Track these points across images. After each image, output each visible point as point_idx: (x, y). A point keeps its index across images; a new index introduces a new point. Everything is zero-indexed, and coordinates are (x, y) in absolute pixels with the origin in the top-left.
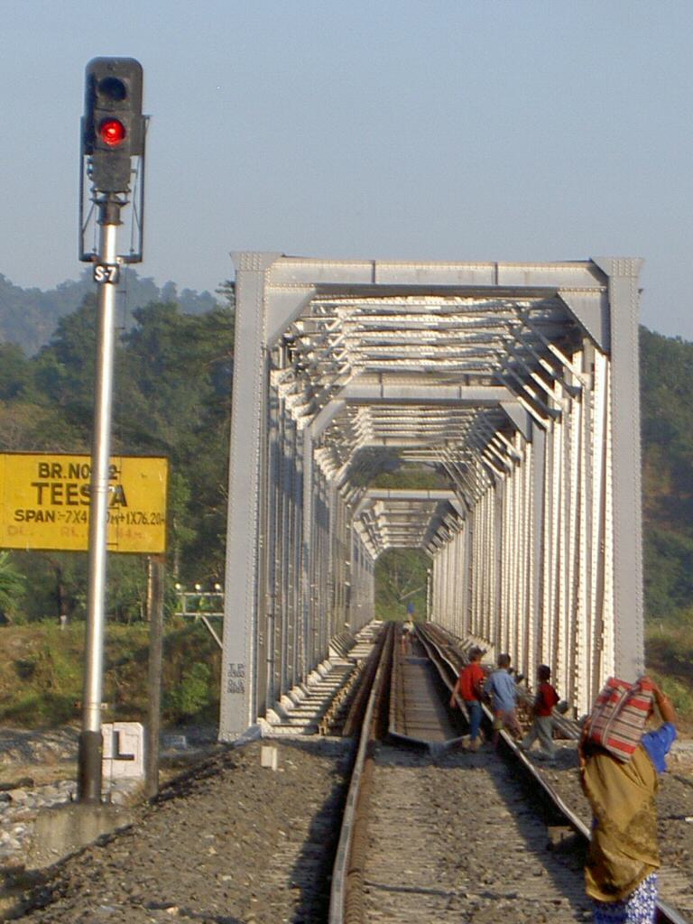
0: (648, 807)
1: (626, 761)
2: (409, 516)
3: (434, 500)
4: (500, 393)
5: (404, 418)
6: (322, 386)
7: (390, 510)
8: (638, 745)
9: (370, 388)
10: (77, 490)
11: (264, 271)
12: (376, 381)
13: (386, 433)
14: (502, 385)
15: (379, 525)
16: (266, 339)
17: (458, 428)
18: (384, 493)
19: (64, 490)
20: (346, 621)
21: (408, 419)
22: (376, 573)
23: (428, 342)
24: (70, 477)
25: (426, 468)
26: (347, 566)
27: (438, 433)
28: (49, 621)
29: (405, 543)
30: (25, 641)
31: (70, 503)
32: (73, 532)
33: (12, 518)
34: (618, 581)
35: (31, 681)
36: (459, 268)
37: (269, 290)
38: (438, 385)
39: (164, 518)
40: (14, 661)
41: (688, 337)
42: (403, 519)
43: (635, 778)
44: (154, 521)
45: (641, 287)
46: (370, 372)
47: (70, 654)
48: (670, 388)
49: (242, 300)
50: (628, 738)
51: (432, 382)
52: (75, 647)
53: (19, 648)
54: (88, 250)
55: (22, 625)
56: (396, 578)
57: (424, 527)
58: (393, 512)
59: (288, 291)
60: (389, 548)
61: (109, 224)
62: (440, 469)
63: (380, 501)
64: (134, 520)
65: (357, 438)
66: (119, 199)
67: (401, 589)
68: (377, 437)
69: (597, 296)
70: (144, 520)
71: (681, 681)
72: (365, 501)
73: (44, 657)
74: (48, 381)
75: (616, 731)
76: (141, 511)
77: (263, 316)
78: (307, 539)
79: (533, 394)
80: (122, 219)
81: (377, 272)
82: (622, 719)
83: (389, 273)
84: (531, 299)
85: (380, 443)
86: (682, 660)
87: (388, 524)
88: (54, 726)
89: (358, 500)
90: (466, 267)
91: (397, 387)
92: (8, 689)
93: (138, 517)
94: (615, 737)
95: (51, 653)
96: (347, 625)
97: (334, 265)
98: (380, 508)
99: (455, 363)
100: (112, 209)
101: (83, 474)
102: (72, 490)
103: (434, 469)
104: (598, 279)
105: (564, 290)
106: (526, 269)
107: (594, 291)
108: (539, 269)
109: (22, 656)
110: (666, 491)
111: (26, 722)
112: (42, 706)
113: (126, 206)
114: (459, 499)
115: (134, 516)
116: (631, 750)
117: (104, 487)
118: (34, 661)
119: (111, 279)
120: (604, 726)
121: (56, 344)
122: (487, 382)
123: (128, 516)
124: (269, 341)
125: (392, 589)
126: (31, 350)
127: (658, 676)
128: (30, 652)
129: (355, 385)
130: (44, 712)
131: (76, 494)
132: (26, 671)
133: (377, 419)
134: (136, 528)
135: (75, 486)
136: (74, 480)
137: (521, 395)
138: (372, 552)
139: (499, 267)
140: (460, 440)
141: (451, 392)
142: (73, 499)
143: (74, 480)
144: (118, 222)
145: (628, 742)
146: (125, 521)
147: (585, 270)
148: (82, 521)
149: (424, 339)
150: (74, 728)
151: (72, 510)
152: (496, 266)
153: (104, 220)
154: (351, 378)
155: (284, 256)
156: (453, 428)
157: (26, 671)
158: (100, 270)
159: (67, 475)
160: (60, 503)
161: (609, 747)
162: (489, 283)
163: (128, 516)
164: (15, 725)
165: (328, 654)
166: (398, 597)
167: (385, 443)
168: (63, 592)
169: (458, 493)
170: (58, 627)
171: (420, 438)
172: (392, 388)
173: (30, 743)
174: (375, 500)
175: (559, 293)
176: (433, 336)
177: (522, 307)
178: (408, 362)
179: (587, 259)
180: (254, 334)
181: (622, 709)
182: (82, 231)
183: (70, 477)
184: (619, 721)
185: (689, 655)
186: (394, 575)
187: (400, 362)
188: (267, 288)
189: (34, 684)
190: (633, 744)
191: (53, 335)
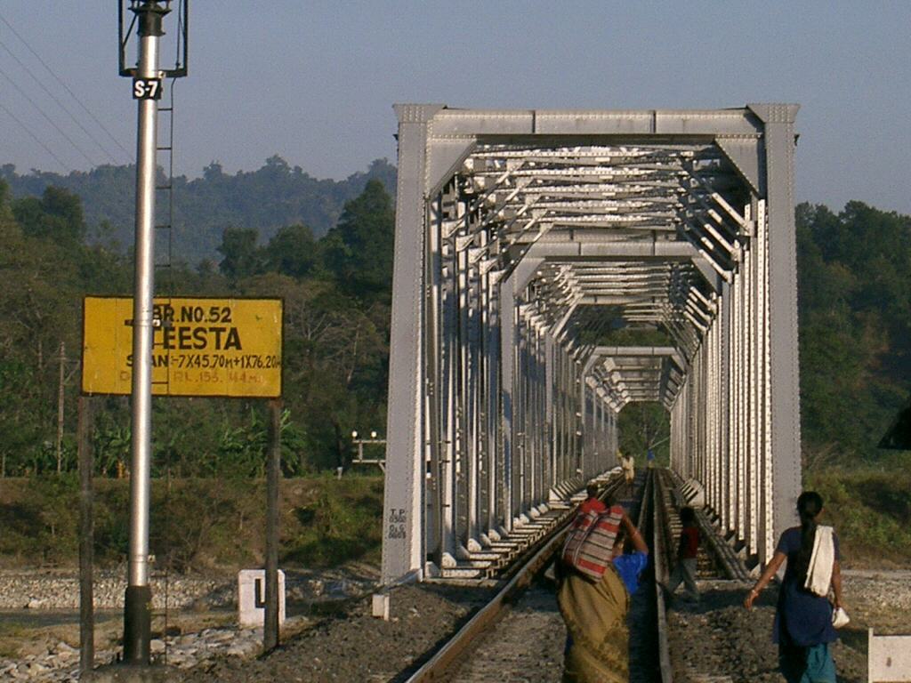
0: (620, 625)
1: (596, 580)
2: (641, 371)
3: (658, 356)
4: (685, 247)
5: (608, 276)
6: (509, 243)
7: (621, 366)
8: (609, 565)
9: (563, 245)
10: (191, 333)
11: (425, 123)
12: (568, 237)
13: (595, 291)
14: (686, 240)
15: (613, 381)
16: (428, 189)
17: (660, 285)
18: (612, 350)
19: (176, 333)
20: (578, 467)
21: (612, 276)
22: (620, 425)
23: (608, 197)
24: (183, 320)
25: (648, 327)
26: (578, 417)
27: (643, 290)
28: (327, 472)
29: (644, 397)
30: (306, 490)
31: (182, 347)
32: (187, 376)
33: (125, 365)
34: (775, 422)
35: (311, 526)
36: (618, 116)
37: (431, 141)
38: (626, 241)
39: (280, 360)
40: (295, 507)
41: (904, 211)
42: (636, 374)
43: (607, 597)
44: (269, 364)
45: (797, 133)
46: (558, 229)
47: (346, 501)
48: (887, 256)
49: (403, 151)
50: (599, 559)
51: (621, 239)
52: (350, 495)
53: (301, 496)
54: (130, 64)
55: (303, 476)
56: (645, 429)
57: (657, 382)
58: (624, 368)
59: (449, 142)
60: (630, 402)
61: (150, 35)
62: (661, 327)
63: (609, 357)
64: (248, 363)
65: (565, 296)
66: (160, 7)
67: (649, 439)
68: (586, 296)
69: (754, 142)
70: (259, 364)
71: (894, 517)
72: (594, 357)
73: (323, 505)
74: (334, 258)
75: (587, 551)
76: (255, 354)
77: (425, 167)
78: (508, 386)
79: (711, 246)
80: (163, 30)
81: (537, 122)
82: (592, 541)
83: (549, 122)
84: (693, 148)
85: (591, 301)
86: (895, 498)
87: (624, 379)
88: (331, 566)
89: (587, 356)
90: (624, 116)
91: (594, 244)
92: (292, 534)
93: (252, 361)
94: (585, 558)
95: (329, 501)
96: (578, 470)
97: (495, 116)
98: (610, 364)
99: (639, 218)
100: (151, 19)
101: (196, 317)
102: (185, 333)
103: (656, 328)
104: (755, 126)
105: (721, 137)
106: (683, 116)
107: (750, 137)
108: (696, 116)
109: (303, 503)
110: (885, 348)
111: (307, 564)
112: (321, 548)
113: (167, 16)
114: (678, 354)
115: (248, 360)
116: (602, 570)
117: (148, 320)
118: (313, 509)
119: (152, 94)
120: (575, 548)
121: (340, 227)
122: (673, 237)
123: (243, 359)
124: (431, 190)
125: (642, 440)
126: (321, 232)
127: (874, 514)
128: (311, 500)
129: (544, 243)
130: (323, 553)
131: (189, 338)
132: (306, 516)
133: (583, 277)
134: (250, 372)
135: (188, 329)
136: (186, 324)
137: (702, 248)
138: (613, 405)
139: (657, 116)
140: (665, 297)
141: (644, 247)
142: (186, 342)
143: (186, 324)
144: (159, 33)
145: (598, 562)
146: (240, 363)
147: (742, 116)
148: (197, 366)
149: (604, 194)
150: (350, 568)
151: (186, 354)
152: (655, 115)
153: (143, 32)
154: (540, 234)
155: (445, 108)
156: (655, 285)
157: (306, 516)
158: (140, 85)
159: (180, 318)
160: (173, 347)
161: (580, 568)
162: (646, 130)
163: (243, 359)
164: (297, 565)
165: (548, 497)
166: (647, 447)
167: (596, 301)
168: (342, 446)
169: (678, 349)
170: (335, 478)
171: (627, 295)
172: (589, 245)
173: (310, 581)
174: (604, 357)
175: (717, 140)
176: (612, 189)
177: (686, 157)
178: (594, 218)
179: (744, 106)
180: (417, 181)
181: (591, 531)
182: (122, 46)
183: (183, 320)
184: (590, 542)
185: (904, 494)
186: (642, 426)
187: (586, 217)
188: (429, 139)
189: (314, 529)
190: (603, 564)
191: (340, 219)
